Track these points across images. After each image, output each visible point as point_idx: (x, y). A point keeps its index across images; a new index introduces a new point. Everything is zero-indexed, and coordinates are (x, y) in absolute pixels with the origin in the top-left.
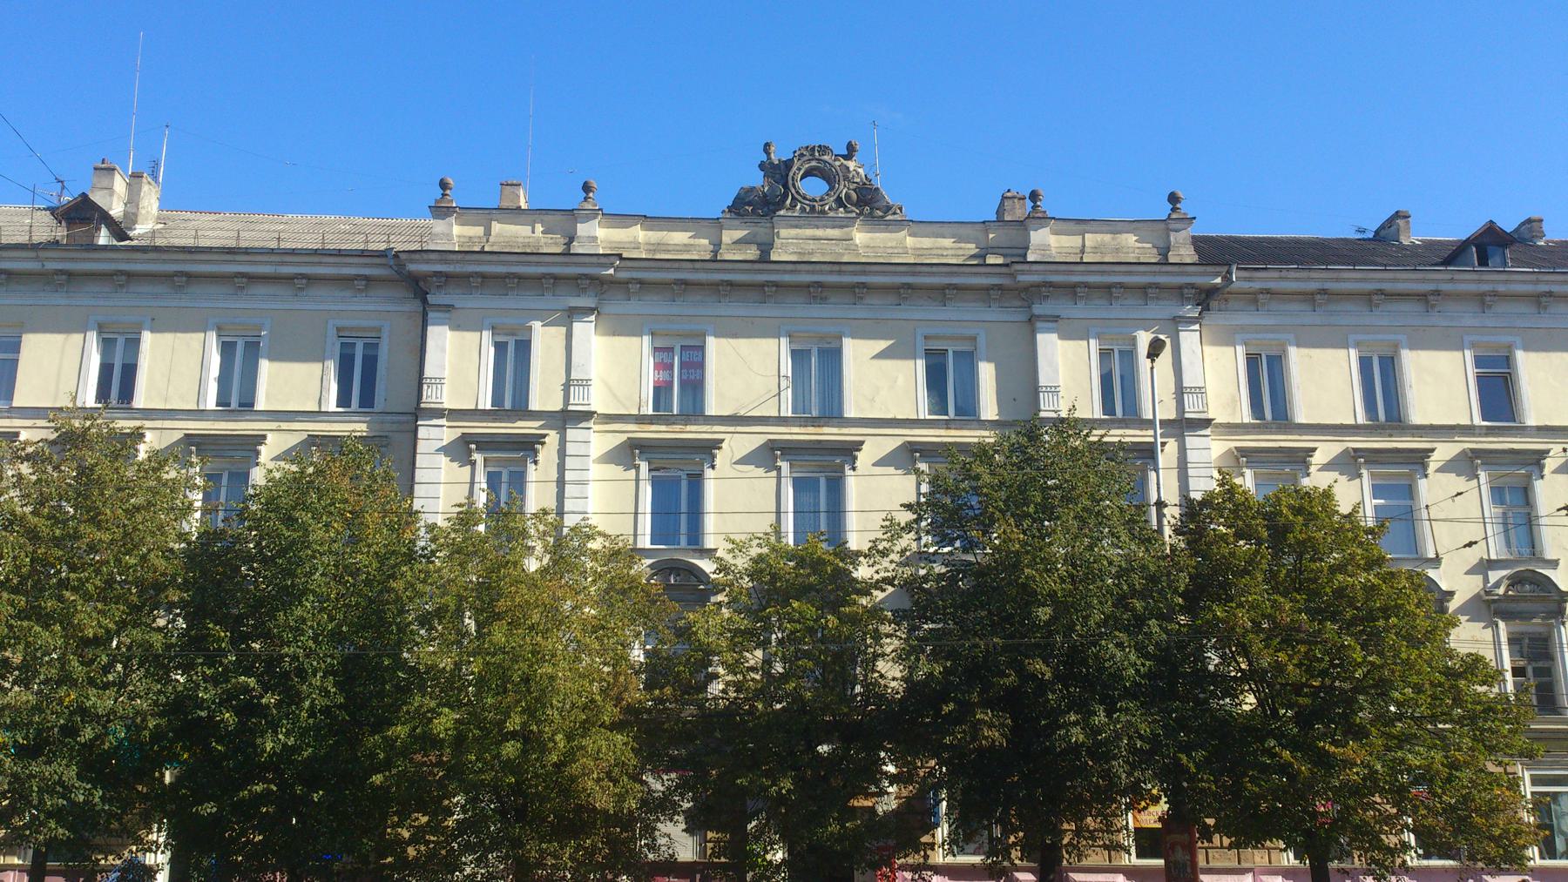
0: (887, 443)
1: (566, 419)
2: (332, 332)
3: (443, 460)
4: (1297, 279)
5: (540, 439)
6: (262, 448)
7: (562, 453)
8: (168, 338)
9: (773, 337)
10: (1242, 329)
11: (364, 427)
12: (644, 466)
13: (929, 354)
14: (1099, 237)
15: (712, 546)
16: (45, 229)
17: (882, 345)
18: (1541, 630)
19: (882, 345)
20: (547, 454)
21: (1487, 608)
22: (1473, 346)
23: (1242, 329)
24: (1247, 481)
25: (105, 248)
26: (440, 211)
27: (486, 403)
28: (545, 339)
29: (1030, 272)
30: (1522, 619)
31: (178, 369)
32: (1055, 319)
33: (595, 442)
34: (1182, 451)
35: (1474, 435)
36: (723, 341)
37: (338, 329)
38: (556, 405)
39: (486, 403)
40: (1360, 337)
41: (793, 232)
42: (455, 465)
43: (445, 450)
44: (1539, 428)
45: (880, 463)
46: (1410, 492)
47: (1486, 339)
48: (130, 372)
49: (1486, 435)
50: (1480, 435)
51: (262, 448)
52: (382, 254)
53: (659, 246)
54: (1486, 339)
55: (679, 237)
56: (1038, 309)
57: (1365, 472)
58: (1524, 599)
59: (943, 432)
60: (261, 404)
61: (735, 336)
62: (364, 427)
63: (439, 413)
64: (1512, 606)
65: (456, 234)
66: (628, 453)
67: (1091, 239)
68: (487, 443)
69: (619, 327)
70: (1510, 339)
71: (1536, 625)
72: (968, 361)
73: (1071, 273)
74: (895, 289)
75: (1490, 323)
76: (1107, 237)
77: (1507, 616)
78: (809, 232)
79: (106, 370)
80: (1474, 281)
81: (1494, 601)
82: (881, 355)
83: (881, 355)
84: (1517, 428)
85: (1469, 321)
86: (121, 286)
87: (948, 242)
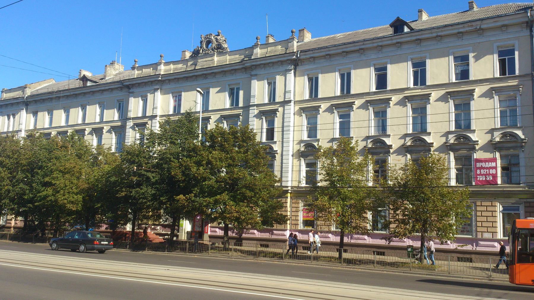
0: (485, 88)
1: (286, 102)
2: (116, 101)
3: (255, 119)
4: (318, 53)
5: (277, 110)
6: (475, 93)
7: (284, 114)
8: (434, 60)
9: (447, 56)
10: (307, 70)
11: (120, 123)
12: (264, 118)
13: (501, 54)
14: (271, 48)
15: (474, 129)
16: (391, 31)
17: (218, 89)
18: (384, 158)
19: (218, 89)
20: (279, 114)
21: (492, 146)
22: (453, 54)
23: (307, 70)
24: (225, 126)
25: (89, 86)
26: (133, 68)
27: (338, 93)
28: (279, 79)
29: (247, 63)
30: (506, 150)
31: (192, 101)
32: (256, 75)
33: (292, 108)
34: (284, 110)
35: (370, 95)
36: (393, 65)
37: (118, 100)
38: (282, 100)
39: (266, 101)
40: (339, 68)
41: (201, 60)
42: (401, 107)
43: (131, 128)
44: (391, 90)
45: (437, 100)
46: (348, 116)
47: (379, 61)
48: (424, 72)
49: (374, 95)
50: (372, 95)
51: (475, 93)
52: (118, 82)
53: (176, 69)
54: (379, 61)
55: (180, 66)
56: (253, 73)
57: (335, 111)
58: (418, 146)
59: (230, 111)
60: (210, 109)
61: (188, 91)
62: (120, 123)
63: (130, 119)
64: (375, 151)
65: (136, 73)
66: (303, 110)
67: (269, 49)
68: (337, 106)
69: (164, 93)
70: (385, 61)
71: (463, 152)
72: (238, 90)
73: (257, 61)
74: (67, 97)
75: (423, 49)
76: (273, 48)
77: (373, 154)
78: (204, 60)
79: (415, 74)
80: (371, 43)
81: (494, 144)
82: (218, 92)
83: (218, 92)
84: (468, 82)
85: (373, 56)
86: (399, 47)
87: (237, 56)
